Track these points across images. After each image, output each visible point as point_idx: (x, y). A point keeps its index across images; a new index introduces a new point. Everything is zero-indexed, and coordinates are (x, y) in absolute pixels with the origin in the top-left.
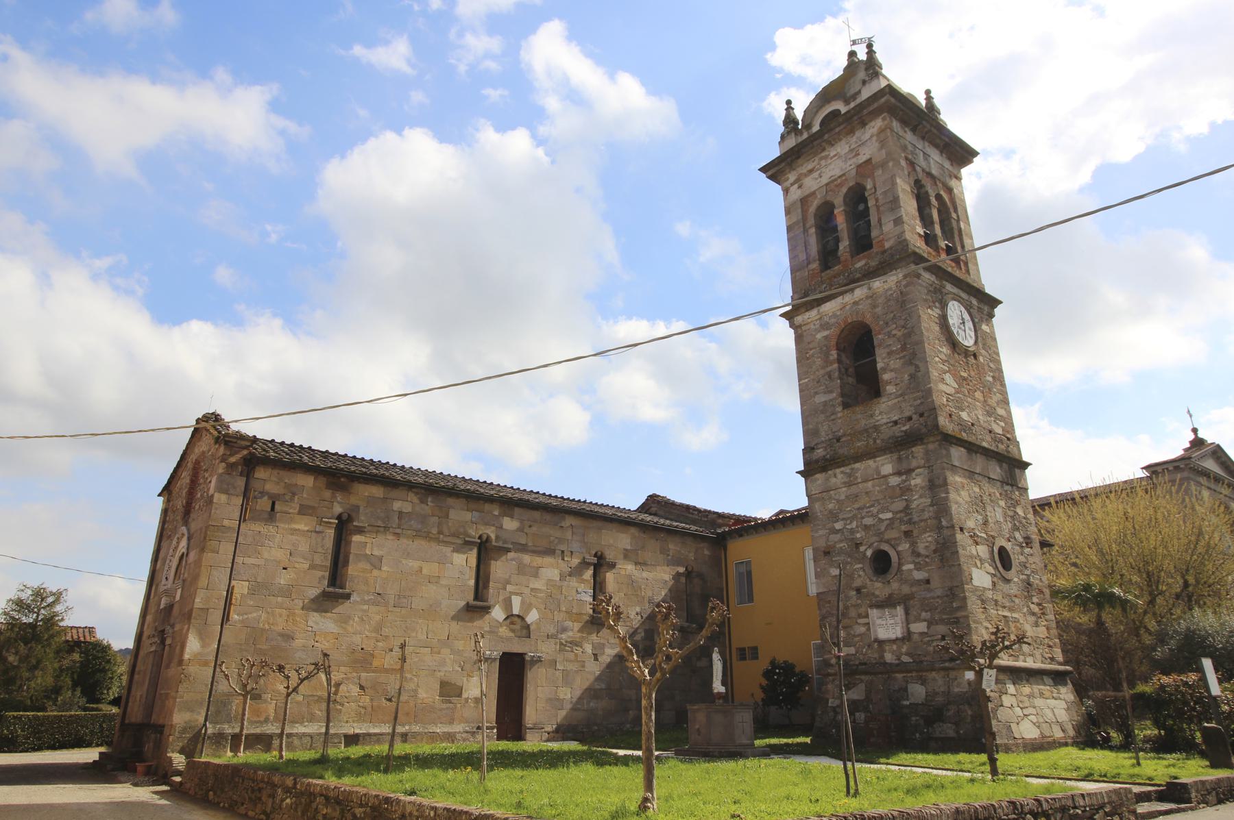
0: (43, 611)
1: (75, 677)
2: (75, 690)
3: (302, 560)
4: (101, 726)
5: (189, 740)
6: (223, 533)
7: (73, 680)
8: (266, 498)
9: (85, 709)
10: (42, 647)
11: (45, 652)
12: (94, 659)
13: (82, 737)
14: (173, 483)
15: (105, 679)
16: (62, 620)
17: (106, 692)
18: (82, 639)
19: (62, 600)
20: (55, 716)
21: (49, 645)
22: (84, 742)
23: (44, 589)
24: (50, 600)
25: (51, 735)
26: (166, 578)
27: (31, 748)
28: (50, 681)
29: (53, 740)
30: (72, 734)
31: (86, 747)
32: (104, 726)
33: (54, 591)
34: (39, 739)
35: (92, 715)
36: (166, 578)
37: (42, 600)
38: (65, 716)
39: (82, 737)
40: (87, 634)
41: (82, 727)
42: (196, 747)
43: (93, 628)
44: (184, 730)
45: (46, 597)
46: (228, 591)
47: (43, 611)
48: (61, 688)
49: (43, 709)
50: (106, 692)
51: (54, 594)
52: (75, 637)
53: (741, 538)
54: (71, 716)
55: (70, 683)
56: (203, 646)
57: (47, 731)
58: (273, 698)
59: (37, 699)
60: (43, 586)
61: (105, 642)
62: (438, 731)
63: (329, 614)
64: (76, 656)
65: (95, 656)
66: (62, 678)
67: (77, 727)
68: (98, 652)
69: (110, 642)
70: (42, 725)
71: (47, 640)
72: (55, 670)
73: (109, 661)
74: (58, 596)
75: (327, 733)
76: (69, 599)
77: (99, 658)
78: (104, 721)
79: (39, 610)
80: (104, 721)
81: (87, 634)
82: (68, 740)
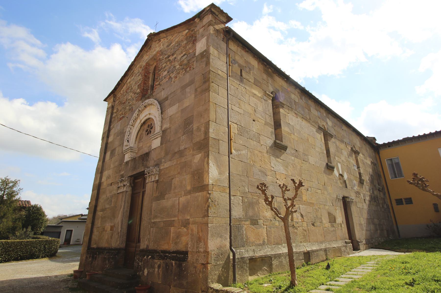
0: (6, 190)
1: (23, 222)
2: (28, 228)
3: (261, 117)
4: (44, 247)
5: (223, 267)
6: (219, 79)
7: (22, 224)
8: (237, 65)
9: (33, 238)
10: (7, 207)
11: (8, 210)
12: (33, 214)
13: (34, 253)
14: (118, 90)
15: (38, 223)
16: (17, 194)
17: (39, 229)
18: (25, 206)
19: (17, 185)
20: (18, 242)
21: (10, 206)
22: (35, 256)
23: (8, 179)
24: (11, 185)
25: (16, 253)
26: (128, 141)
27: (4, 260)
28: (10, 224)
29: (17, 255)
30: (28, 252)
31: (36, 259)
32: (46, 246)
33: (13, 180)
34: (9, 255)
35: (39, 241)
36: (128, 141)
37: (7, 185)
38: (24, 242)
39: (34, 253)
40: (27, 204)
41: (34, 247)
42: (229, 274)
43: (29, 201)
44: (218, 255)
45: (9, 183)
46: (228, 128)
47: (6, 190)
48: (16, 227)
49: (8, 238)
50: (39, 229)
51: (13, 182)
52: (21, 204)
53: (390, 148)
54: (28, 242)
55: (21, 225)
56: (220, 174)
57: (13, 250)
58: (265, 223)
59: (3, 233)
60: (8, 178)
61: (38, 206)
62: (335, 246)
63: (279, 160)
64: (23, 213)
65: (34, 212)
66: (17, 223)
67: (31, 248)
68: (35, 210)
69: (41, 206)
70: (10, 247)
71: (9, 204)
72: (13, 219)
73: (40, 215)
74: (15, 183)
75: (290, 253)
76: (21, 185)
77: (35, 213)
78: (46, 244)
79: (5, 190)
80: (46, 244)
81: (27, 204)
82: (26, 255)
